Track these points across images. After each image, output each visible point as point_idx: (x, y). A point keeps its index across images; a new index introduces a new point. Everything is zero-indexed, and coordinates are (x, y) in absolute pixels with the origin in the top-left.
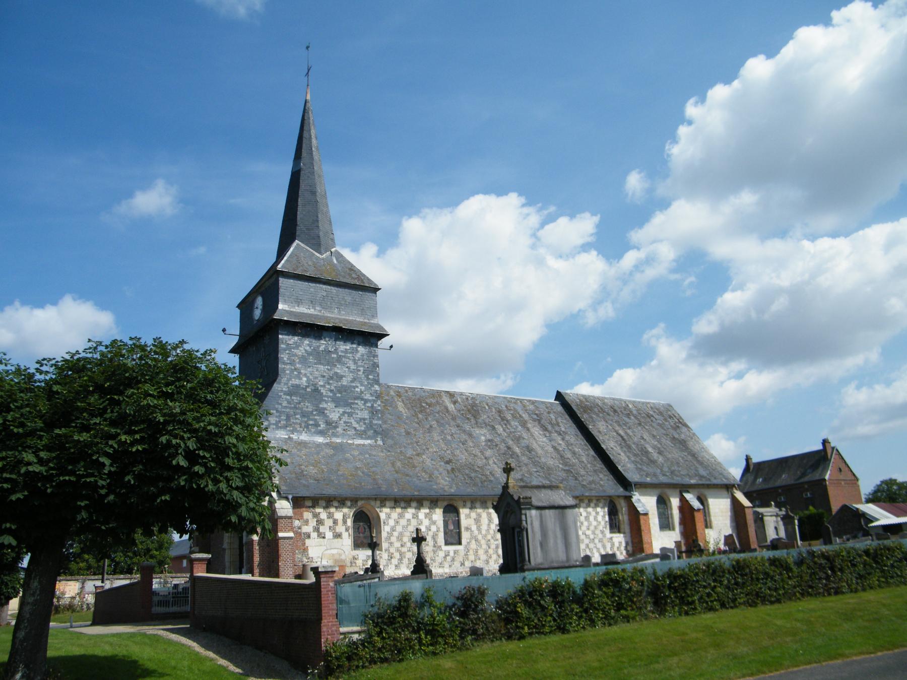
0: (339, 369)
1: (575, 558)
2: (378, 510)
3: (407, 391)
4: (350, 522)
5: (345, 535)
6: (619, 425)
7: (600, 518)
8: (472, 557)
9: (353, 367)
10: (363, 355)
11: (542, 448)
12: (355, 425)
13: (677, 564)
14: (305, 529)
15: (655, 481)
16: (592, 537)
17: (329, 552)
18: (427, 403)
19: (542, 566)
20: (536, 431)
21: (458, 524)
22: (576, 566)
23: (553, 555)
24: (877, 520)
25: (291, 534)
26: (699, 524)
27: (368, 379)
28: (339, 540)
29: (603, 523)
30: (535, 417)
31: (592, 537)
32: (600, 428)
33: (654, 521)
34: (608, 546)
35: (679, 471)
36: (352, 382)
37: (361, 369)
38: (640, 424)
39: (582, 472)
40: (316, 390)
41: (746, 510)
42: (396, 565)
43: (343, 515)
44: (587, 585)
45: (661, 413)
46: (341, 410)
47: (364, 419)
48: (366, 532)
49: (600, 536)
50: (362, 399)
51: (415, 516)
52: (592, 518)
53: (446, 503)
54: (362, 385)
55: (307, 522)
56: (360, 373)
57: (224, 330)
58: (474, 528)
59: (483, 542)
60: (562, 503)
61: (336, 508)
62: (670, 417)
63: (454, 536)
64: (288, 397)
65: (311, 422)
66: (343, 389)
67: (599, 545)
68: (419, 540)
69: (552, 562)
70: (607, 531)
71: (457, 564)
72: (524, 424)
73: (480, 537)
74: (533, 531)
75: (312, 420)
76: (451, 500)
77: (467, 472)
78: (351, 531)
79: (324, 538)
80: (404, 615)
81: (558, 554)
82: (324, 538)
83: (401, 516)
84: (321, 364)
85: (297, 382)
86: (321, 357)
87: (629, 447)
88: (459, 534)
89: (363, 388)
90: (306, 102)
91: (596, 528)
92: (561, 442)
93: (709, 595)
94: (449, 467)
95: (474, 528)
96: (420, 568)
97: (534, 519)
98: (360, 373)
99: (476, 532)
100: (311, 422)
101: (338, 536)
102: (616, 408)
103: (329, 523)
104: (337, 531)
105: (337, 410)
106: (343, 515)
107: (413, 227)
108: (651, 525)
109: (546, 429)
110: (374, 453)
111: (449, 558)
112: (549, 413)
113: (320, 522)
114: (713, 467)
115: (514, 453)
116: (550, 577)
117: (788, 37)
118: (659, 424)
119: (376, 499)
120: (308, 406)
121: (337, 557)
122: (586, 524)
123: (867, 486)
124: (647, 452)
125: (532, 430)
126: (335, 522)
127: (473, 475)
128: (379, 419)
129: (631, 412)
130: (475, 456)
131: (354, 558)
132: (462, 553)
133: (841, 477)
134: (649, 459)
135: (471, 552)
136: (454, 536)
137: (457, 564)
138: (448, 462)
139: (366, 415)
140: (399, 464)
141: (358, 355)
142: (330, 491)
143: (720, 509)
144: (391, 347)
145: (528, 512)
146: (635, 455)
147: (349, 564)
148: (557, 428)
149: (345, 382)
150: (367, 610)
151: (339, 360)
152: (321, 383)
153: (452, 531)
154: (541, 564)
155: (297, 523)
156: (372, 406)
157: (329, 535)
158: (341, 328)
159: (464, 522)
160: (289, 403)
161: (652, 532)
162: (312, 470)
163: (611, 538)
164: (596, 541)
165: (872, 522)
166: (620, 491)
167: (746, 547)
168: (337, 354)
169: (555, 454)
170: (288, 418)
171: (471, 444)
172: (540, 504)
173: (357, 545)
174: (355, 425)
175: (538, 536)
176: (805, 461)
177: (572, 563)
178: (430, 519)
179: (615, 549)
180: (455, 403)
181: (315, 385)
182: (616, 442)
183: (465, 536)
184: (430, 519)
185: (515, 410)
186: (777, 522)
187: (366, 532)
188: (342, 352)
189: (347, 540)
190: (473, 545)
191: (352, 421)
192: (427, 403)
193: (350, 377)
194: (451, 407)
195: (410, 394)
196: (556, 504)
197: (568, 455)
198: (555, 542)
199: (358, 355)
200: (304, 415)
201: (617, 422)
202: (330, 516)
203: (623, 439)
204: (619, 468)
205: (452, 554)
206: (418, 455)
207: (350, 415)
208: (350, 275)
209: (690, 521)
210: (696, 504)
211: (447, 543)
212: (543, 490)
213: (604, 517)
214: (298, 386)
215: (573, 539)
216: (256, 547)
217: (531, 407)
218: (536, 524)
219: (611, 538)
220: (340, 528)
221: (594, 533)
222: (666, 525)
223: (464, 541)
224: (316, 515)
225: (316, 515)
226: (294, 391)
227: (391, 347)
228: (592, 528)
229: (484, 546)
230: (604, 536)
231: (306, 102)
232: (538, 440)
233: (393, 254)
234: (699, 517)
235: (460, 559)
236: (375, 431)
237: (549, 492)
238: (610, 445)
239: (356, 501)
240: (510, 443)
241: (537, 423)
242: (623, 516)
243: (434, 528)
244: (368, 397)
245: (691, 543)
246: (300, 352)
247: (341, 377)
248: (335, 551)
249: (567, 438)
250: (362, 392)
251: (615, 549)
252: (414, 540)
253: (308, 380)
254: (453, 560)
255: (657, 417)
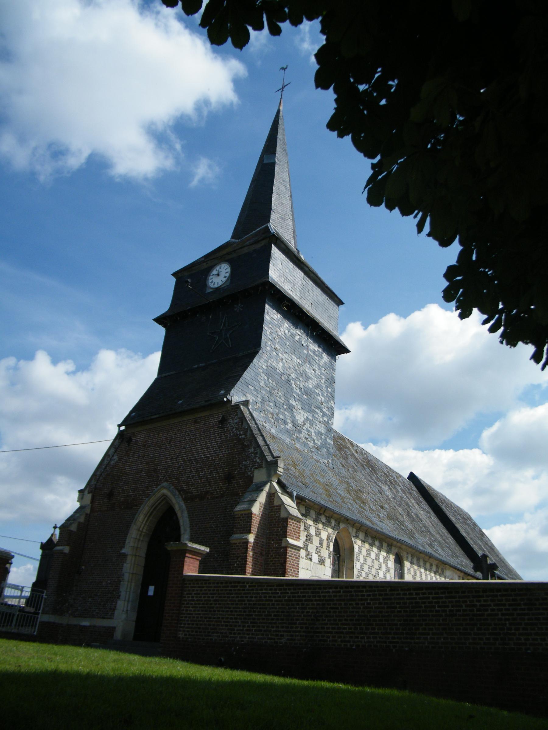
2: (353, 540)
54: (323, 395)
61: (324, 524)
90: (279, 111)
98: (323, 381)
107: (107, 358)
117: (420, 306)
149: (311, 384)
157: (315, 558)
160: (266, 384)
199: (322, 362)
216: (250, 553)
226: (271, 372)
231: (279, 111)
233: (84, 377)
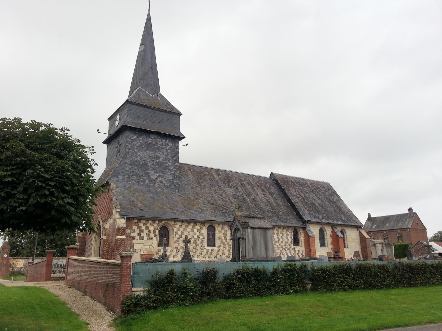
0: (158, 154)
1: (271, 257)
3: (194, 168)
4: (157, 232)
5: (154, 238)
6: (302, 192)
7: (289, 238)
8: (221, 253)
9: (165, 153)
10: (171, 147)
11: (261, 200)
12: (164, 182)
13: (326, 264)
14: (133, 234)
15: (319, 221)
16: (284, 247)
17: (145, 247)
18: (204, 174)
19: (253, 260)
20: (259, 191)
21: (214, 235)
22: (271, 261)
23: (258, 254)
24: (436, 250)
25: (124, 237)
26: (341, 245)
27: (173, 159)
28: (151, 241)
29: (290, 240)
30: (259, 184)
31: (284, 247)
32: (292, 193)
33: (317, 241)
34: (293, 252)
35: (331, 217)
36: (164, 160)
37: (170, 154)
38: (312, 192)
39: (281, 213)
40: (145, 163)
41: (367, 240)
42: (175, 255)
43: (154, 227)
44: (275, 272)
45: (324, 187)
46: (158, 175)
47: (170, 180)
48: (164, 237)
49: (289, 247)
50: (170, 170)
51: (192, 230)
52: (284, 237)
53: (209, 225)
55: (134, 231)
56: (169, 156)
57: (98, 130)
58: (223, 238)
59: (227, 246)
60: (265, 226)
62: (329, 190)
63: (211, 242)
64: (130, 166)
65: (141, 180)
66: (159, 164)
67: (288, 252)
68: (187, 242)
69: (258, 258)
70: (292, 245)
71: (213, 256)
72: (253, 188)
73: (226, 243)
74: (248, 241)
75: (142, 178)
76: (212, 223)
77: (221, 209)
78: (158, 237)
79: (143, 239)
80: (170, 282)
81: (262, 253)
82: (143, 239)
83: (185, 230)
84: (148, 150)
85: (135, 159)
86: (148, 147)
87: (306, 203)
88: (215, 241)
89: (170, 164)
91: (286, 242)
92: (271, 198)
93: (342, 282)
94: (212, 207)
95: (223, 238)
96: (187, 257)
97: (250, 234)
98: (169, 156)
99: (224, 240)
100: (141, 180)
101: (150, 239)
102: (301, 183)
103: (146, 231)
104: (150, 236)
105: (155, 174)
106: (154, 227)
108: (316, 243)
109: (264, 191)
110: (173, 197)
111: (209, 253)
112: (266, 183)
113: (141, 231)
114: (351, 216)
115: (246, 201)
116: (259, 266)
118: (322, 193)
119: (172, 220)
120: (140, 172)
121: (149, 250)
122: (281, 240)
123: (430, 234)
124: (315, 206)
125: (257, 191)
126: (149, 231)
127: (224, 211)
128: (177, 180)
129: (309, 186)
130: (226, 202)
131: (158, 251)
132: (216, 251)
133: (418, 228)
134: (316, 210)
135: (221, 250)
136: (211, 242)
137: (213, 256)
138: (212, 204)
139: (171, 177)
140: (186, 203)
141: (168, 147)
142: (147, 215)
143: (352, 238)
144: (187, 144)
145: (246, 230)
146: (309, 207)
147: (155, 254)
148: (269, 191)
149: (160, 160)
150: (150, 279)
151: (158, 149)
152: (148, 160)
153: (211, 239)
154: (252, 258)
155: (129, 231)
156: (174, 173)
157: (146, 238)
158: (160, 133)
159: (218, 235)
161: (316, 247)
162: (139, 204)
163: (294, 248)
164: (286, 249)
165: (433, 251)
166: (300, 224)
167: (366, 257)
168: (157, 146)
169: (267, 204)
170: (129, 177)
171: (225, 196)
172: (253, 226)
173: (160, 244)
174: (164, 182)
175: (251, 243)
176: (399, 218)
177: (269, 259)
178: (200, 232)
179: (296, 254)
180: (218, 175)
181: (144, 161)
182: (300, 200)
183: (218, 242)
184: (200, 232)
185: (249, 180)
186: (383, 247)
187: (164, 237)
188: (160, 145)
189: (155, 241)
190: (222, 247)
191: (164, 180)
192: (204, 174)
193: (163, 158)
194: (216, 177)
195: (196, 169)
196: (262, 227)
197: (274, 204)
198: (261, 248)
199: (168, 147)
200: (137, 175)
201: (301, 190)
202: (147, 228)
203: (303, 199)
204: (300, 212)
205: (210, 251)
206: (197, 199)
207: (162, 177)
208: (167, 106)
209: (338, 242)
210: (340, 234)
211: (208, 245)
212: (256, 220)
213: (291, 237)
214: (135, 161)
215: (270, 246)
217: (257, 180)
218: (251, 237)
219: (294, 248)
220: (152, 235)
221: (285, 245)
222: (323, 244)
223: (217, 245)
224: (139, 227)
225: (139, 227)
227: (187, 144)
228: (284, 242)
229: (228, 248)
230: (291, 247)
232: (261, 197)
234: (341, 241)
235: (214, 253)
236: (175, 186)
237: (258, 220)
238: (296, 201)
239: (162, 221)
240: (245, 196)
241: (259, 188)
242: (302, 239)
243: (202, 237)
244: (172, 169)
245: (337, 254)
246: (138, 143)
247: (159, 157)
248: (148, 247)
249: (274, 196)
250: (169, 166)
251: (296, 254)
252: (184, 242)
253: (141, 158)
254: (211, 254)
255: (322, 189)
